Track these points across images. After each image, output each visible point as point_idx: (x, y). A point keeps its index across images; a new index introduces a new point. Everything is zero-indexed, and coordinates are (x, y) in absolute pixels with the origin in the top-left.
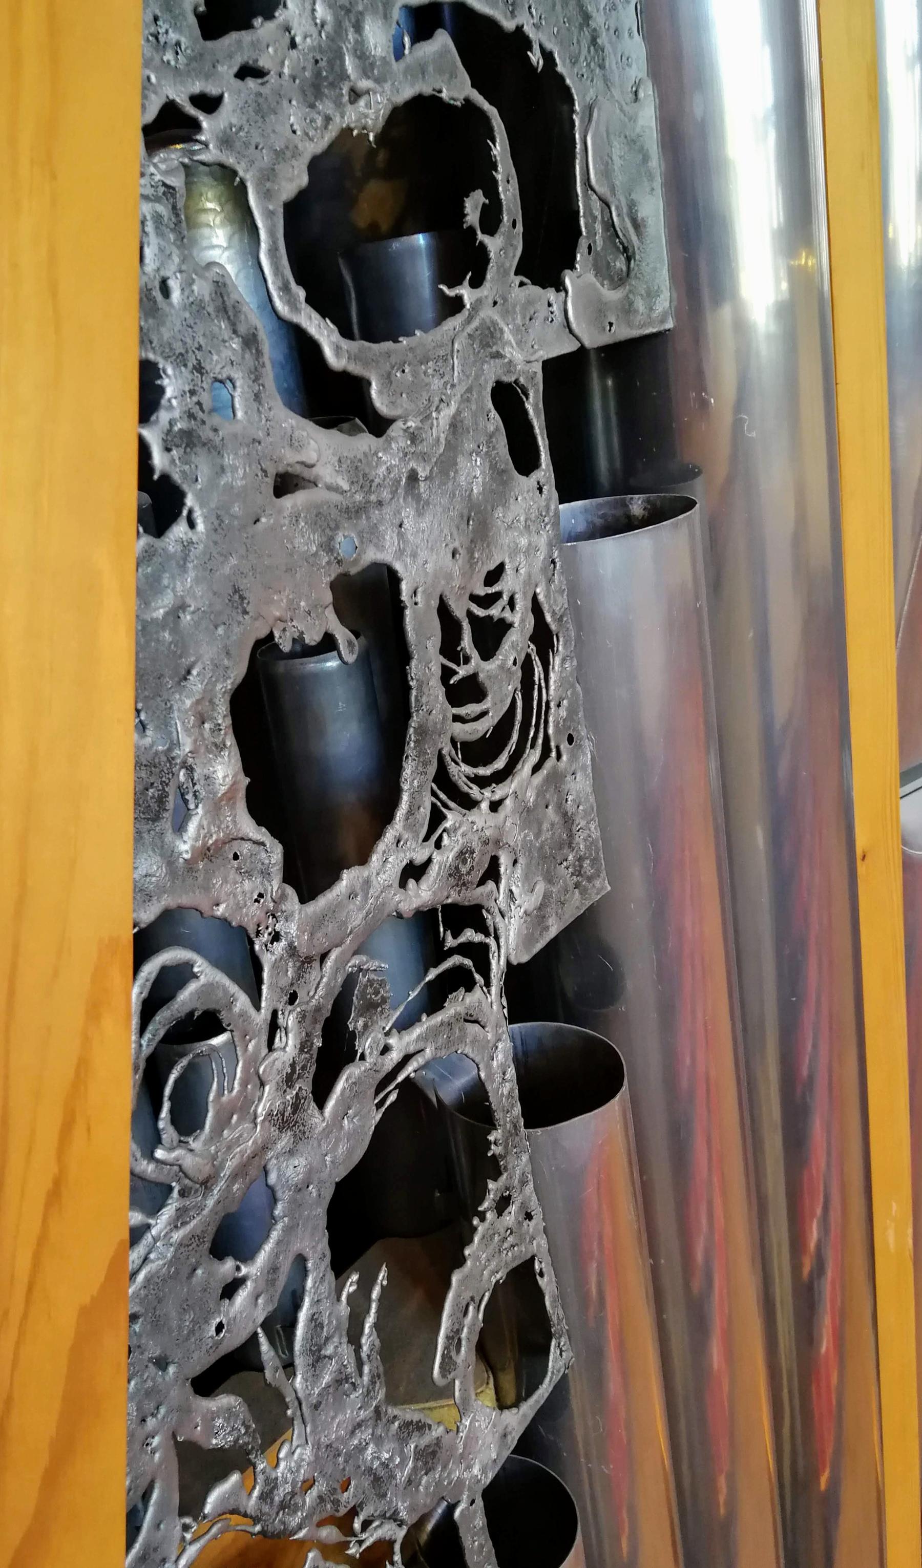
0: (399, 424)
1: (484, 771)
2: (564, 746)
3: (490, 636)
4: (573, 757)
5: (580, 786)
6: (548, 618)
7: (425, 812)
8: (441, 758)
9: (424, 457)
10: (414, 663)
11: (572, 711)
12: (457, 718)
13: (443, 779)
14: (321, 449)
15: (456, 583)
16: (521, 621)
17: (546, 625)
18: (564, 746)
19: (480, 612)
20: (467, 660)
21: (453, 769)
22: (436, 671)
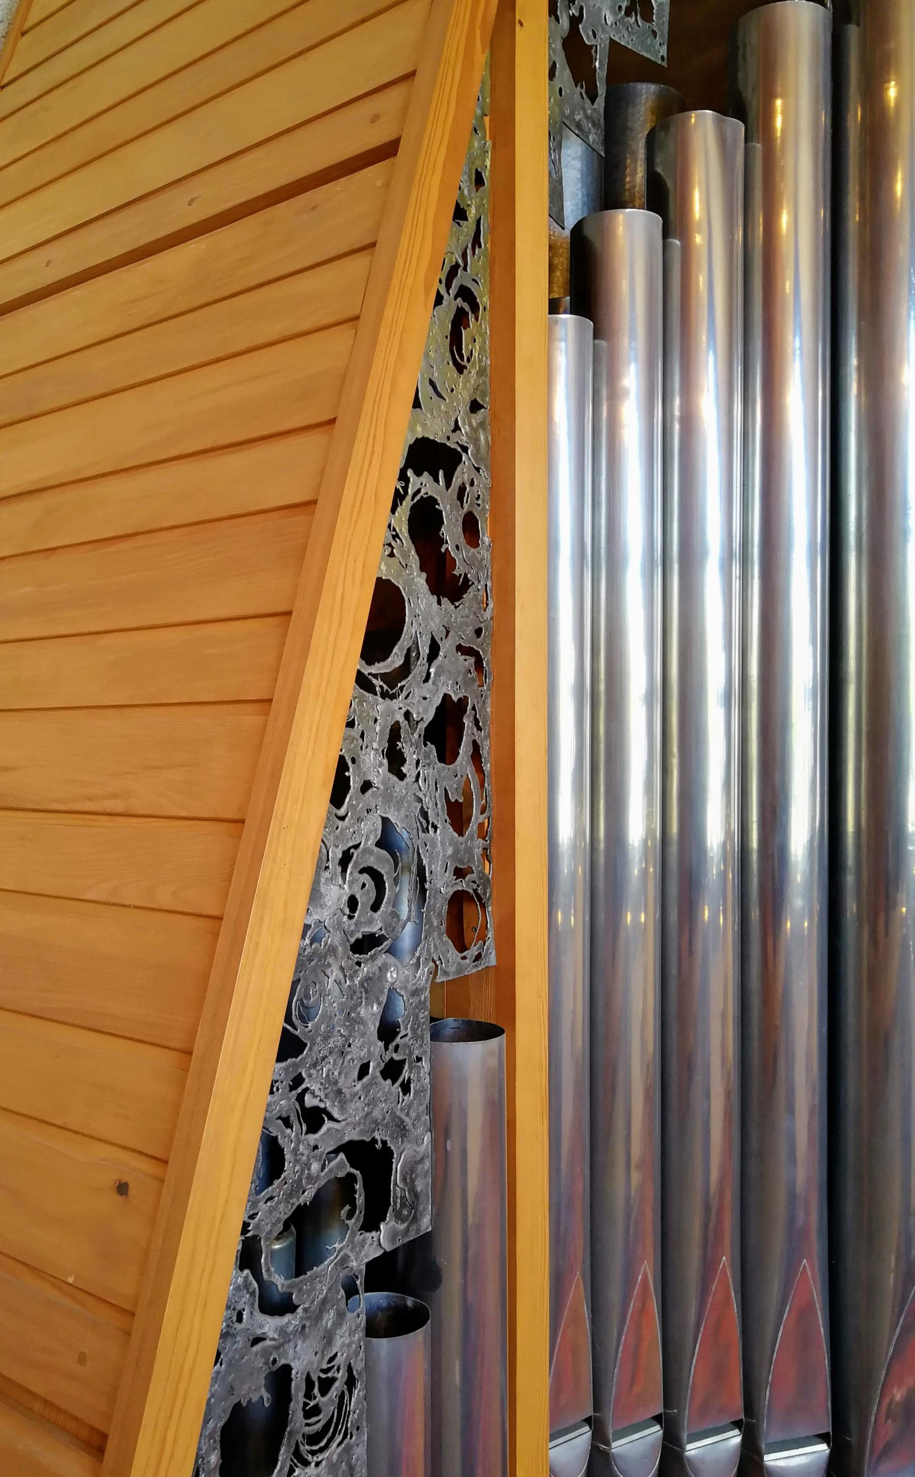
0: (302, 1306)
1: (315, 1448)
2: (355, 1432)
3: (326, 1385)
4: (359, 1437)
5: (360, 1452)
6: (355, 1373)
7: (286, 1470)
8: (297, 1443)
9: (309, 1318)
10: (292, 1403)
11: (360, 1415)
12: (307, 1425)
13: (297, 1454)
14: (270, 1325)
15: (315, 1366)
16: (341, 1376)
17: (353, 1376)
18: (355, 1432)
19: (323, 1376)
20: (315, 1398)
21: (302, 1448)
22: (301, 1405)
